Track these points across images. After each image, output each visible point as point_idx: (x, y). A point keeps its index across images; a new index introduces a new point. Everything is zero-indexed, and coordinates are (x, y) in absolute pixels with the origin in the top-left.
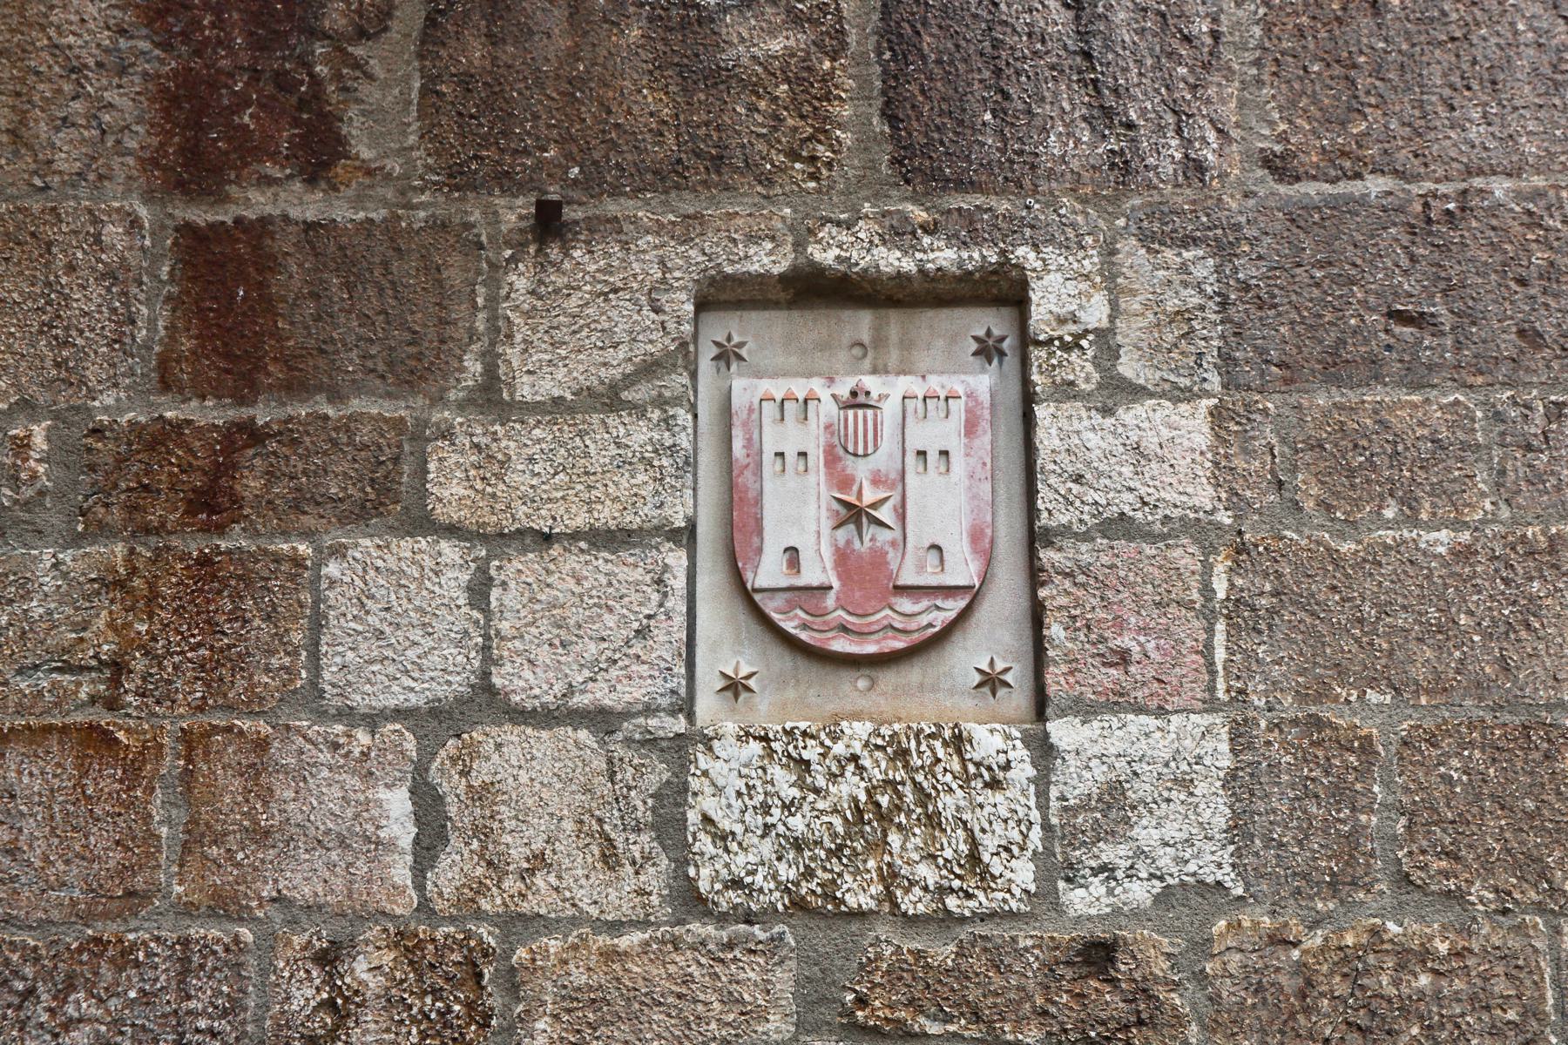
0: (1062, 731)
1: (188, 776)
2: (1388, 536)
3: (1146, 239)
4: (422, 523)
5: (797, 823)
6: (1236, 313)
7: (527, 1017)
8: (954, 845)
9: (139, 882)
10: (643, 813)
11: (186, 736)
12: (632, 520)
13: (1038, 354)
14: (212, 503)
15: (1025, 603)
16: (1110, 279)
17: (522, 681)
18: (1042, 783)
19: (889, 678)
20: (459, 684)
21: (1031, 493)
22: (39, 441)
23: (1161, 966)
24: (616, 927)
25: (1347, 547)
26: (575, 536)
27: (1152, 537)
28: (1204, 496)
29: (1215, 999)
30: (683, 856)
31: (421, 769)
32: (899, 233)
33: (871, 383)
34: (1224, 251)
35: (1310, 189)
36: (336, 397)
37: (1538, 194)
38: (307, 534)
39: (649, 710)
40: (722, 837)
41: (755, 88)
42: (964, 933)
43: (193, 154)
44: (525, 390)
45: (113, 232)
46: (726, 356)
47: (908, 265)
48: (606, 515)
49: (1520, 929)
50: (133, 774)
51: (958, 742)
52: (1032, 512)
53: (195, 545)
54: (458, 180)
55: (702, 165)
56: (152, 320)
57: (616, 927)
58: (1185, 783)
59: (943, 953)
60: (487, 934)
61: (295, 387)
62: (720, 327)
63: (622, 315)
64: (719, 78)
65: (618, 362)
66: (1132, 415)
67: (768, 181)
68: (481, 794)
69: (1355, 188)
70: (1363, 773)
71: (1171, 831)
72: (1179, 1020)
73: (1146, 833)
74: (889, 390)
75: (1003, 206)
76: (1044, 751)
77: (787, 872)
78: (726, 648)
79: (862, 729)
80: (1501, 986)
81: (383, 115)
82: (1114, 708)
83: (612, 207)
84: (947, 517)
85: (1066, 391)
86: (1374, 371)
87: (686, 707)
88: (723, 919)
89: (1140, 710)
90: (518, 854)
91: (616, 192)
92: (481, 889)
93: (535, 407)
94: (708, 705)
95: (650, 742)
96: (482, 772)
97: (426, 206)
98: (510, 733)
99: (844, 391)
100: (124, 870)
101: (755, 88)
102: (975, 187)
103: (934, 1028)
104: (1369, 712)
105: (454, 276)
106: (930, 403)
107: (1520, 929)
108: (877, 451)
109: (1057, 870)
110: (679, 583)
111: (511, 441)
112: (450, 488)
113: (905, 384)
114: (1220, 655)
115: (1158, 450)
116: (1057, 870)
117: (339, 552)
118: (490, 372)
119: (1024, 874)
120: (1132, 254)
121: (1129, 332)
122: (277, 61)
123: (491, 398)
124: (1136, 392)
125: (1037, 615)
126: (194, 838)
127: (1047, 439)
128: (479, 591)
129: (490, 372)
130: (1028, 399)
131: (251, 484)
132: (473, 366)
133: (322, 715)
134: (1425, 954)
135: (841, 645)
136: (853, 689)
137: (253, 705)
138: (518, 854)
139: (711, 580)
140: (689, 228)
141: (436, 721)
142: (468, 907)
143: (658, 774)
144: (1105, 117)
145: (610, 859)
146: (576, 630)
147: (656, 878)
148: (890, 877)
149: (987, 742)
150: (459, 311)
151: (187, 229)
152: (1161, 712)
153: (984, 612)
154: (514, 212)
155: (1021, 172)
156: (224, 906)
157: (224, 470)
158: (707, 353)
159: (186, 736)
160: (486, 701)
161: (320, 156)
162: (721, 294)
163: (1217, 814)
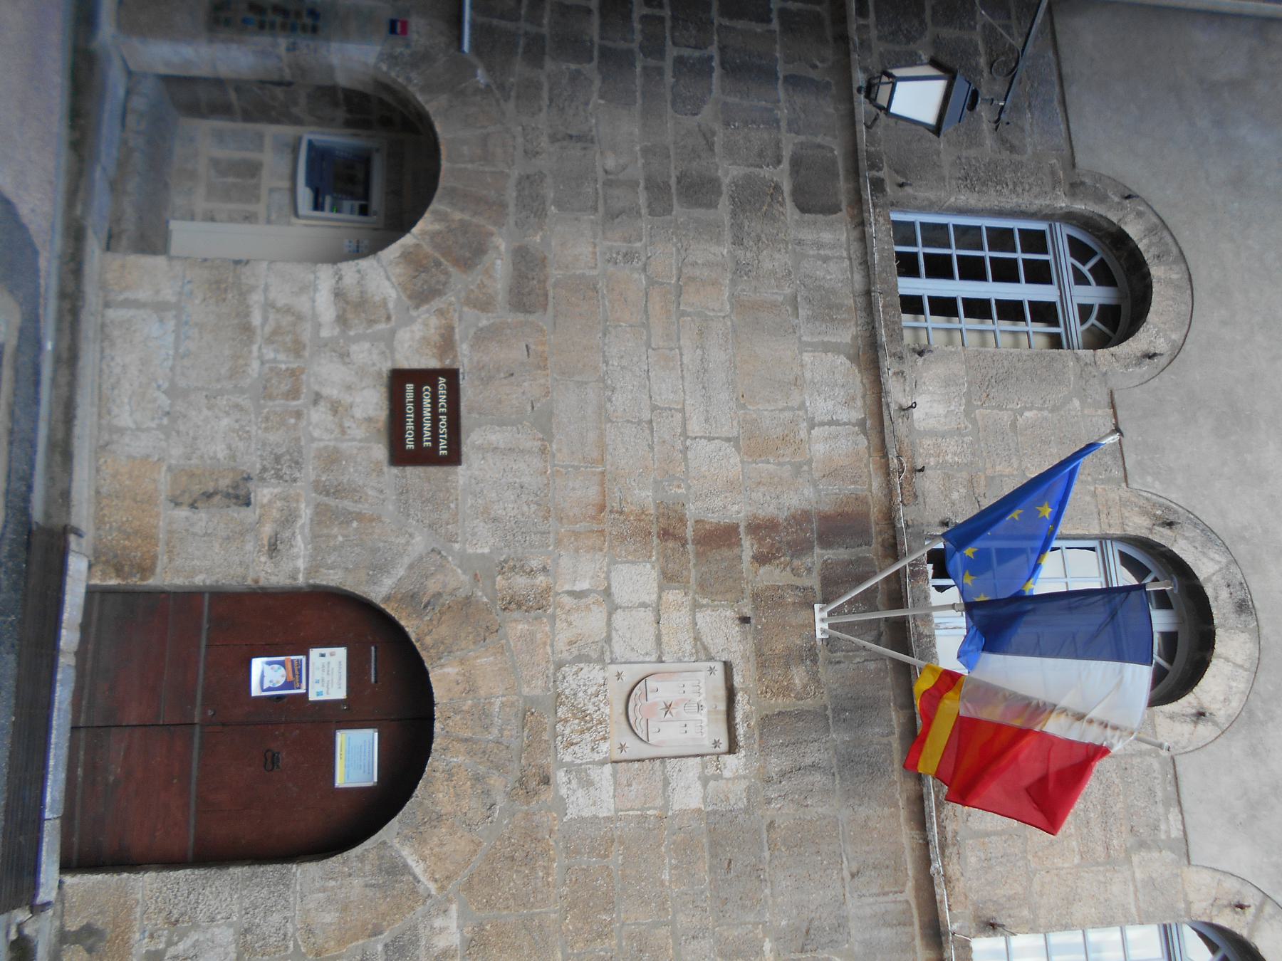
0: (608, 768)
1: (593, 531)
2: (667, 861)
3: (749, 788)
4: (661, 589)
5: (581, 694)
6: (729, 815)
7: (528, 622)
8: (576, 738)
9: (565, 521)
10: (583, 651)
11: (603, 531)
12: (663, 646)
13: (715, 758)
14: (666, 534)
15: (644, 756)
16: (737, 778)
17: (618, 617)
18: (593, 763)
19: (623, 718)
20: (618, 600)
21: (675, 757)
22: (680, 491)
23: (543, 798)
24: (552, 646)
25: (663, 849)
26: (659, 630)
27: (664, 793)
28: (676, 807)
29: (534, 814)
30: (572, 663)
31: (595, 591)
32: (747, 717)
33: (705, 710)
34: (746, 811)
35: (765, 835)
36: (695, 565)
37: (766, 902)
38: (658, 559)
39: (612, 652)
40: (576, 674)
41: (786, 675)
42: (551, 741)
43: (758, 527)
44: (699, 615)
45: (736, 507)
46: (711, 670)
47: (738, 720)
48: (665, 639)
49: (556, 902)
50: (593, 518)
51: (604, 738)
52: (670, 758)
53: (654, 529)
54: (756, 596)
55: (763, 661)
56: (713, 518)
57: (552, 646)
58: (594, 804)
59: (545, 737)
60: (550, 611)
61: (698, 555)
62: (719, 668)
63: (720, 641)
64: (787, 666)
65: (707, 640)
66: (698, 785)
67: (760, 679)
68: (588, 608)
69: (766, 848)
70: (599, 855)
71: (581, 800)
72: (528, 803)
73: (580, 793)
74: (703, 716)
75: (756, 746)
76: (602, 763)
77: (567, 692)
78: (631, 673)
79: (607, 711)
80: (540, 896)
81: (772, 576)
82: (615, 783)
83: (750, 637)
84: (669, 735)
85: (705, 767)
86: (714, 856)
87: (613, 662)
88: (554, 674)
89: (615, 790)
90: (571, 618)
91: (754, 638)
92: (562, 608)
93: (694, 618)
94: (613, 669)
95: (603, 653)
96: (594, 608)
97: (749, 589)
98: (604, 615)
99: (703, 703)
100: (568, 516)
101: (786, 675)
102: (761, 738)
103: (525, 734)
104: (617, 857)
105: (728, 596)
106: (705, 728)
107: (556, 902)
108: (685, 713)
109: (569, 768)
110: (647, 659)
111: (685, 611)
112: (673, 596)
113: (705, 720)
114: (631, 813)
115: (688, 795)
116: (569, 768)
117: (653, 567)
118: (703, 606)
119: (568, 758)
120: (744, 784)
121: (722, 783)
122: (785, 548)
123: (696, 606)
124: (705, 786)
125: (643, 760)
126: (576, 534)
127: (691, 761)
128: (644, 605)
129: (703, 606)
130: (702, 756)
131: (671, 544)
132: (705, 601)
133: (609, 565)
134: (548, 874)
135: (631, 704)
136: (620, 708)
137: (611, 547)
138: (571, 618)
139: (649, 668)
140: (746, 658)
141: (607, 592)
142: (560, 605)
143: (594, 655)
144: (783, 774)
145: (571, 643)
146: (634, 631)
147: (565, 655)
148: (566, 721)
149: (604, 747)
150: (719, 597)
151: (738, 526)
152: (614, 796)
153: (643, 745)
154: (747, 611)
155: (765, 750)
156: (558, 542)
157: (675, 537)
158: (712, 664)
159: (603, 531)
160: (613, 609)
161: (761, 559)
162: (728, 668)
163: (587, 813)
